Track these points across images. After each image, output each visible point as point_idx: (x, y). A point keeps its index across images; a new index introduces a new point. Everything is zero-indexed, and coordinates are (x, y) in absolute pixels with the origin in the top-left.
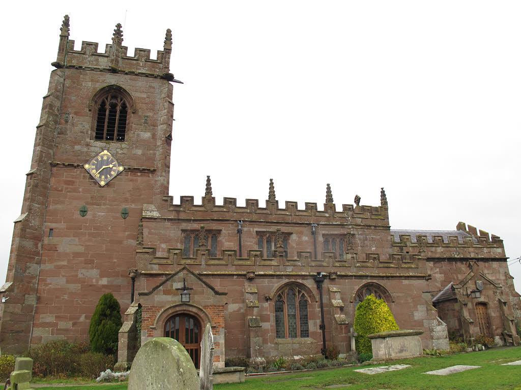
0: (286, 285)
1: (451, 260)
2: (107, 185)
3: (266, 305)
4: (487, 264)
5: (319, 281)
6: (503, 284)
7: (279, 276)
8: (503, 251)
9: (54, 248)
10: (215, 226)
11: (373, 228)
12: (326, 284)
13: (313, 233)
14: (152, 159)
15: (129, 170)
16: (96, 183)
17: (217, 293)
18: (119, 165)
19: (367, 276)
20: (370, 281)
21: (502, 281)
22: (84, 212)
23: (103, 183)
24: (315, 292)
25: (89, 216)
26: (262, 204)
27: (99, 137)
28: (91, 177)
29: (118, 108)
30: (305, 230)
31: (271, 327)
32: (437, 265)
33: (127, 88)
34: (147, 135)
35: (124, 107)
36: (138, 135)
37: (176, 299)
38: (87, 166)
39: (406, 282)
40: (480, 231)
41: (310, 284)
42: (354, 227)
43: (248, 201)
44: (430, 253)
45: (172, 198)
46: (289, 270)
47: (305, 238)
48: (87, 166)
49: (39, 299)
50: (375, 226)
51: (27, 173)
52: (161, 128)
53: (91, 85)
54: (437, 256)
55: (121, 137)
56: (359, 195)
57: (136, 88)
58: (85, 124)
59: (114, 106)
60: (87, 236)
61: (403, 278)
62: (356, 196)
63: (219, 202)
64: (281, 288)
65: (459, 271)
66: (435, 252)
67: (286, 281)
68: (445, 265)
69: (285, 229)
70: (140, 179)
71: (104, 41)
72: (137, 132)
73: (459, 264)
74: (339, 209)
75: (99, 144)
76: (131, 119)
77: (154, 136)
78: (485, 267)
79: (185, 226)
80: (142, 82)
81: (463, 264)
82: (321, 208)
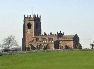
5: (43, 44)
41: (42, 44)
58: (27, 27)
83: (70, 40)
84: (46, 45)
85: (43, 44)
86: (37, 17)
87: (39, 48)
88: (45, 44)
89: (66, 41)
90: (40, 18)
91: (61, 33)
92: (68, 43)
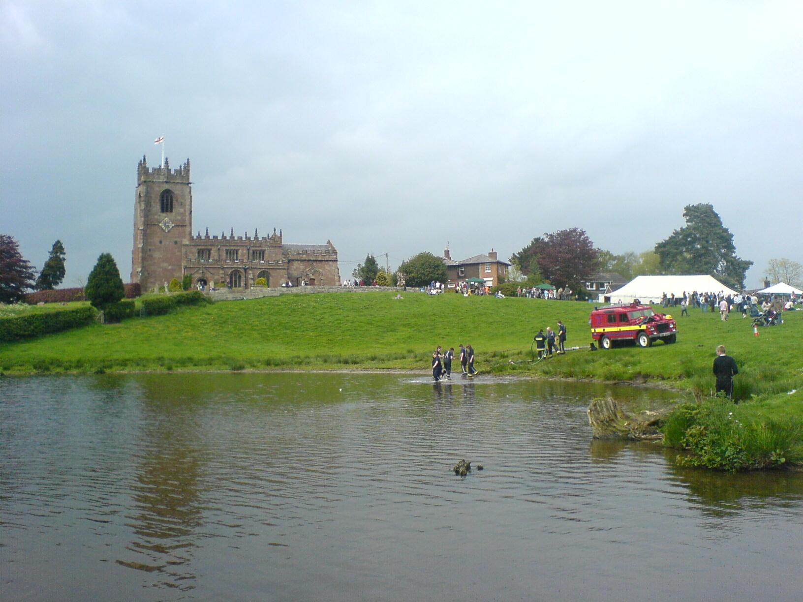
0: (234, 271)
2: (169, 231)
3: (227, 277)
5: (245, 270)
7: (231, 268)
8: (337, 257)
9: (151, 256)
10: (209, 247)
12: (247, 271)
13: (248, 250)
14: (184, 220)
15: (176, 226)
16: (164, 231)
17: (211, 274)
18: (172, 223)
19: (262, 268)
22: (161, 242)
23: (167, 231)
24: (244, 273)
25: (163, 243)
26: (228, 238)
27: (163, 211)
28: (162, 229)
30: (245, 248)
33: (170, 189)
34: (182, 210)
35: (171, 197)
36: (179, 211)
37: (201, 275)
38: (160, 225)
39: (278, 270)
41: (242, 271)
43: (214, 237)
45: (193, 237)
46: (235, 266)
47: (245, 252)
48: (160, 225)
49: (148, 274)
51: (692, 203)
52: (188, 207)
53: (158, 190)
55: (171, 211)
56: (682, 215)
57: (176, 190)
58: (157, 207)
59: (167, 197)
62: (58, 242)
63: (211, 238)
64: (232, 272)
67: (234, 269)
68: (305, 263)
69: (237, 248)
70: (180, 229)
72: (177, 209)
74: (260, 239)
75: (164, 215)
76: (175, 202)
77: (185, 211)
79: (198, 247)
80: (179, 187)
82: (252, 239)
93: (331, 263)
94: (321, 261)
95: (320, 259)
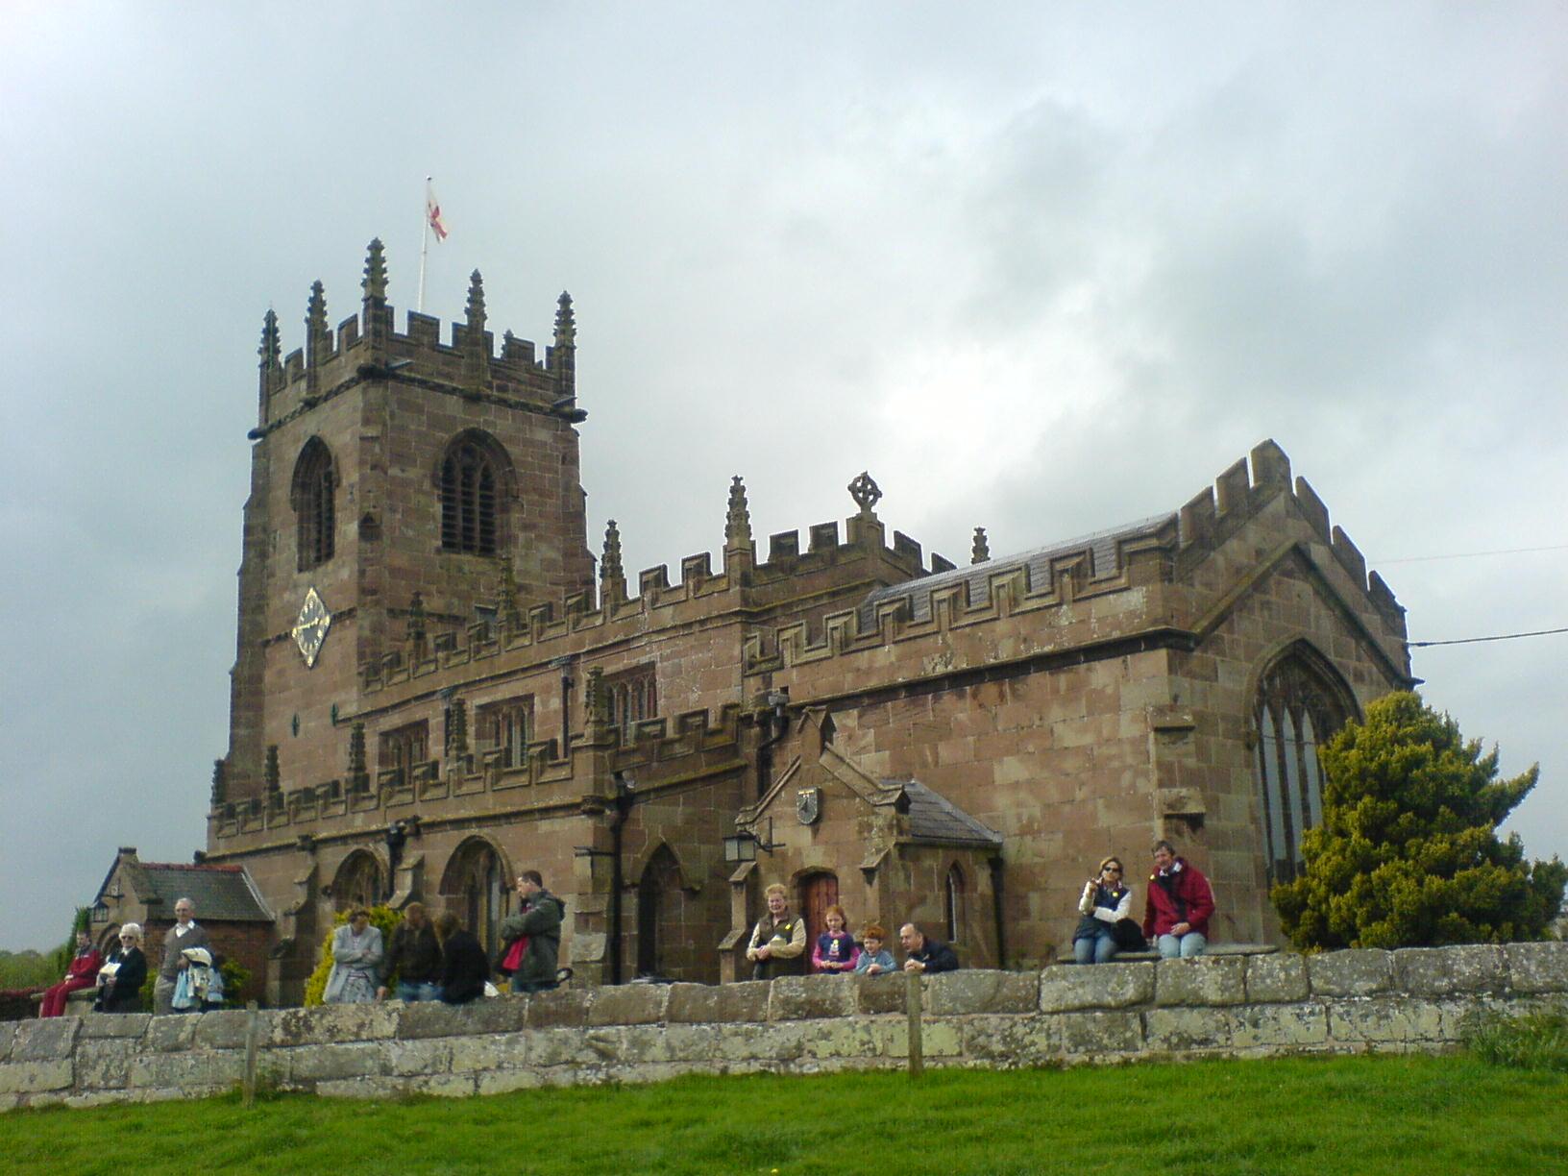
1: (919, 688)
4: (1063, 680)
6: (1130, 760)
11: (696, 628)
15: (335, 619)
20: (355, 847)
21: (1127, 748)
22: (295, 727)
23: (310, 661)
29: (478, 477)
31: (710, 877)
32: (872, 717)
39: (545, 826)
40: (898, 536)
41: (382, 852)
42: (655, 638)
44: (850, 677)
50: (702, 622)
54: (873, 683)
60: (1236, 636)
61: (537, 816)
65: (943, 731)
66: (869, 671)
68: (895, 715)
71: (450, 314)
73: (948, 698)
78: (1056, 691)
81: (961, 696)
83: (1069, 625)
84: (439, 850)
85: (397, 843)
86: (377, 308)
87: (477, 542)
88: (418, 828)
89: (960, 710)
90: (563, 354)
91: (866, 526)
92: (1011, 769)
93: (1102, 674)
94: (1012, 671)
95: (1005, 654)
